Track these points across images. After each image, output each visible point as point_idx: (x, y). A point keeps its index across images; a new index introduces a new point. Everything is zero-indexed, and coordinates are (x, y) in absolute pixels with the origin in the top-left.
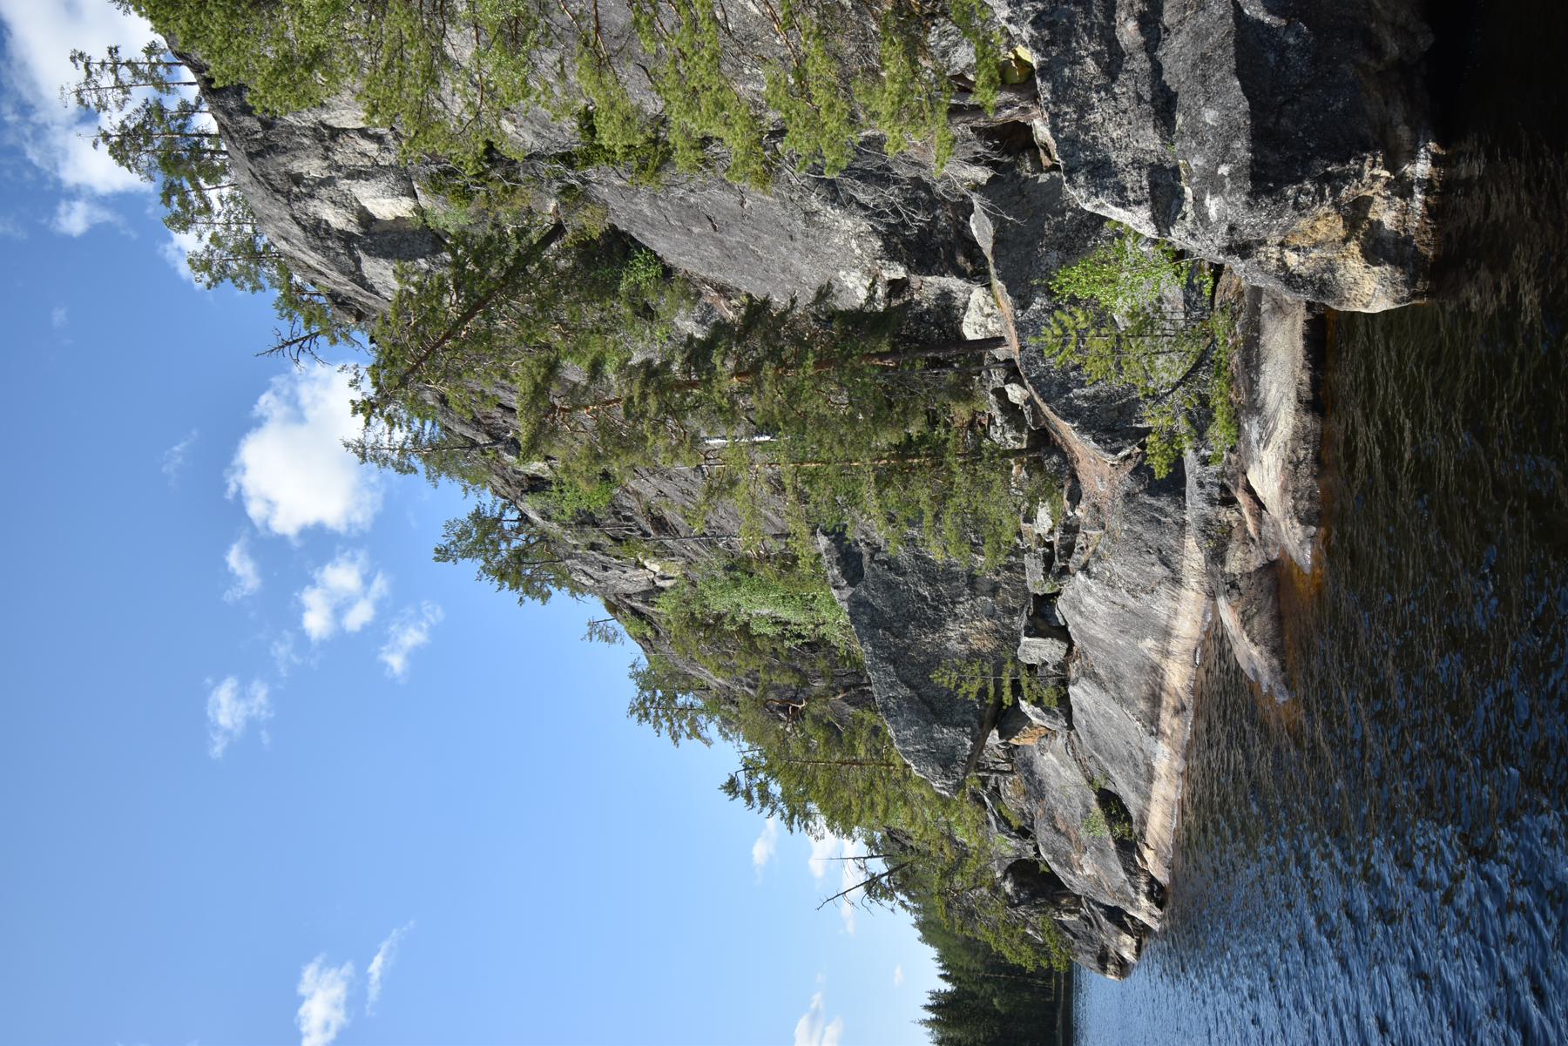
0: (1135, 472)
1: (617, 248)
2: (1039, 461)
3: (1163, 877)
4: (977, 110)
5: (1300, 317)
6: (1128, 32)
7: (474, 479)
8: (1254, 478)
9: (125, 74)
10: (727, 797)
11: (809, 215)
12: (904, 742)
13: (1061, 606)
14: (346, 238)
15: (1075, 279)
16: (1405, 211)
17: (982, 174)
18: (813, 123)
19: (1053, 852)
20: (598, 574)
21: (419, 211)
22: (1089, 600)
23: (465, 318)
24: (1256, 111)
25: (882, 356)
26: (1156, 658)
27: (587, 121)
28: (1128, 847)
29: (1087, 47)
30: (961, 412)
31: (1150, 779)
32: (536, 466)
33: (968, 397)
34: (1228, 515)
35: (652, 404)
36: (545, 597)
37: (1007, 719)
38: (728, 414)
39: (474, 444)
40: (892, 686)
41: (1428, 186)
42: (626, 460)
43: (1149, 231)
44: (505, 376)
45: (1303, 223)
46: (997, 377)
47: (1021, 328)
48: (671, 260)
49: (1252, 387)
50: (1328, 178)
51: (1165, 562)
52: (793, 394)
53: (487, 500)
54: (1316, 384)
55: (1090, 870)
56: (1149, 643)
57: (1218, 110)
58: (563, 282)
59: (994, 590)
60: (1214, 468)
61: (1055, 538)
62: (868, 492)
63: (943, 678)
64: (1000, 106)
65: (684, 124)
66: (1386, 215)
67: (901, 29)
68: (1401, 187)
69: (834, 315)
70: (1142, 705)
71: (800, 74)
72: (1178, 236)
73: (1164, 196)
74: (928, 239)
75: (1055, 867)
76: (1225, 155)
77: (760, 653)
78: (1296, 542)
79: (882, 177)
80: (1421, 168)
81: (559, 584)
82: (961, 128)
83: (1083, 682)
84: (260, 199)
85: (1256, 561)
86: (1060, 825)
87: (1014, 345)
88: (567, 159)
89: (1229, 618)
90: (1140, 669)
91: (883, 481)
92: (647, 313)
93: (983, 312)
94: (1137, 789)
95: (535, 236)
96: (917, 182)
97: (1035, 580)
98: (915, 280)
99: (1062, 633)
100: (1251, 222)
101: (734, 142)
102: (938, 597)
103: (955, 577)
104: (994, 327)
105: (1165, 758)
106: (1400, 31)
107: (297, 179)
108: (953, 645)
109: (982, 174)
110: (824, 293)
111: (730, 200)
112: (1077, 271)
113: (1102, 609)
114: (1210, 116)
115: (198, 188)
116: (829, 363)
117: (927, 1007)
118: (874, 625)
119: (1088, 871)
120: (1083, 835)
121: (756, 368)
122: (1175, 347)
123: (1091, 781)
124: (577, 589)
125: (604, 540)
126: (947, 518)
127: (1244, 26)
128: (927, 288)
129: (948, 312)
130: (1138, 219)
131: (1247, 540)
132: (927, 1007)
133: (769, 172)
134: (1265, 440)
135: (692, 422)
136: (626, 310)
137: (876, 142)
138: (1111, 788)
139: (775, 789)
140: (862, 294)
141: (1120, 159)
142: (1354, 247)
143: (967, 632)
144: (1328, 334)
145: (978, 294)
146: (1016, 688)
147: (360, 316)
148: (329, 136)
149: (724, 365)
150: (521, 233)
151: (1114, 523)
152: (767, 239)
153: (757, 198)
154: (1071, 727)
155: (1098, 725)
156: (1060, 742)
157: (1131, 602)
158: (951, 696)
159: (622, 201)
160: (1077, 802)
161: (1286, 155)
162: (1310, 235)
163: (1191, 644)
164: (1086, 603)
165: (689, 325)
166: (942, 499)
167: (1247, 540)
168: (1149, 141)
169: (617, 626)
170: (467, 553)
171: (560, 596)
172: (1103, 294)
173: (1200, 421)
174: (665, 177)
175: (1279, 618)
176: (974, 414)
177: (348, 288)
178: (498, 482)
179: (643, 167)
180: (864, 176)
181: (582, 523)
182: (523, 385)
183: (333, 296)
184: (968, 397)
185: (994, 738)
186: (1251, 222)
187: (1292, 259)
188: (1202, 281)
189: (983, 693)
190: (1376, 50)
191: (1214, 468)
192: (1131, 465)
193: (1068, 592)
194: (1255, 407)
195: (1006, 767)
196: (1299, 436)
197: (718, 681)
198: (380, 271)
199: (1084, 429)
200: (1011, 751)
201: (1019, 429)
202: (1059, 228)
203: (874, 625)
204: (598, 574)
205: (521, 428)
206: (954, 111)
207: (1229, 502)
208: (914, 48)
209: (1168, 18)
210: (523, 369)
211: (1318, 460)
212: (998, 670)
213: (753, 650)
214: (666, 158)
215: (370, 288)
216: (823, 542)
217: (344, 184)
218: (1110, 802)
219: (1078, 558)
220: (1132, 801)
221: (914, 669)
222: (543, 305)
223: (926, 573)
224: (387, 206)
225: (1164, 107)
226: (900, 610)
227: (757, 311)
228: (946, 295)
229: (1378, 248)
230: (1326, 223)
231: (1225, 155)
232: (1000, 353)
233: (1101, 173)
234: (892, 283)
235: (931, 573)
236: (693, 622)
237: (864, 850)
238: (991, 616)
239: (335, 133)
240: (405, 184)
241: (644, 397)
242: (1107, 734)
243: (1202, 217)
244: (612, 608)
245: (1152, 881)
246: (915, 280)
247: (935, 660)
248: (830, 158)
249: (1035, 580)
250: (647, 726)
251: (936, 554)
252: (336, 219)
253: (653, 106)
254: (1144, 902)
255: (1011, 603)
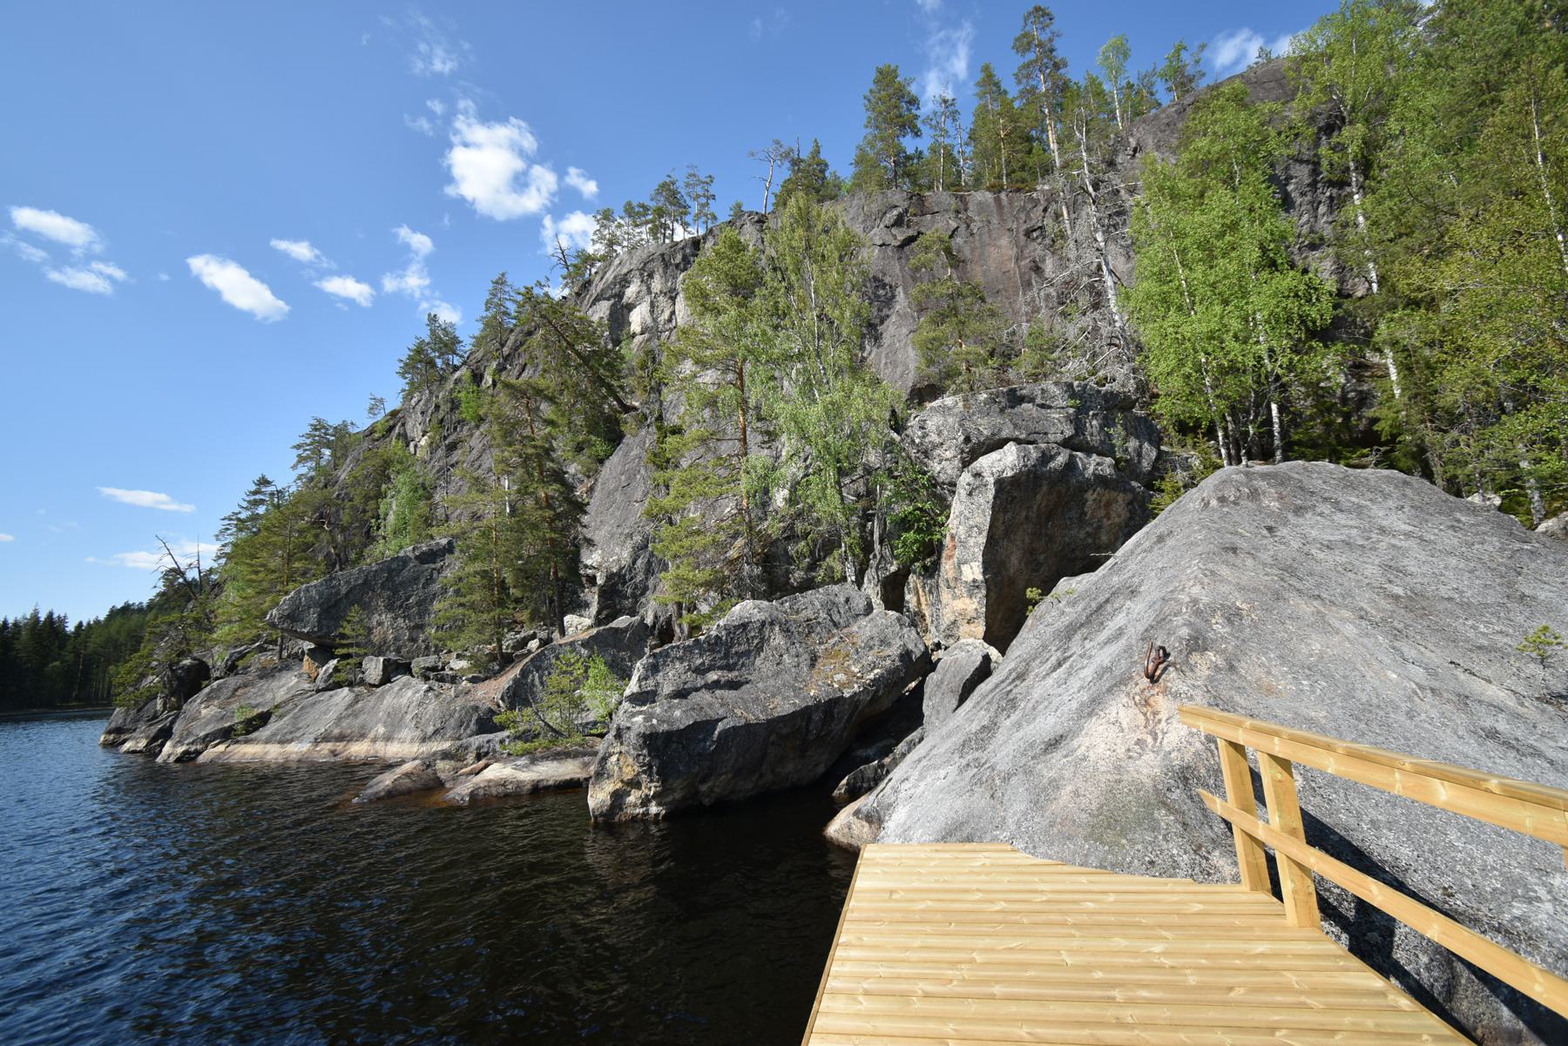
0: (490, 710)
1: (615, 438)
2: (495, 659)
3: (202, 759)
4: (680, 615)
5: (582, 775)
6: (713, 676)
7: (479, 342)
8: (495, 766)
9: (703, 200)
10: (256, 478)
11: (631, 536)
12: (307, 590)
13: (406, 678)
14: (620, 295)
15: (599, 667)
16: (635, 806)
17: (649, 620)
18: (675, 539)
19: (219, 688)
20: (419, 408)
21: (634, 335)
22: (410, 693)
23: (578, 354)
24: (680, 732)
25: (556, 573)
26: (371, 735)
27: (677, 431)
28: (226, 735)
29: (707, 659)
30: (524, 616)
31: (281, 742)
32: (488, 380)
33: (532, 619)
34: (471, 757)
35: (530, 451)
36: (403, 375)
37: (323, 652)
38: (523, 492)
39: (503, 346)
40: (347, 582)
41: (646, 814)
42: (498, 435)
43: (627, 692)
44: (545, 371)
45: (630, 760)
46: (543, 634)
47: (572, 644)
48: (607, 463)
49: (546, 758)
50: (651, 767)
51: (436, 732)
52: (535, 526)
53: (467, 345)
54: (547, 788)
55: (204, 712)
56: (381, 730)
57: (680, 716)
58: (596, 406)
59: (413, 640)
60: (498, 747)
61: (447, 671)
62: (478, 566)
63: (354, 613)
64: (681, 627)
65: (676, 476)
66: (634, 797)
67: (716, 579)
68: (645, 802)
69: (578, 548)
70: (336, 731)
71: (698, 533)
72: (626, 705)
73: (642, 698)
74: (617, 593)
75: (207, 690)
76: (661, 721)
77: (366, 503)
78: (461, 791)
79: (649, 571)
80: (654, 809)
81: (411, 383)
82: (672, 609)
83: (352, 695)
84: (640, 255)
85: (442, 776)
86: (240, 692)
87: (562, 641)
88: (660, 418)
89: (407, 767)
90: (362, 727)
91: (485, 574)
92: (579, 449)
93: (578, 625)
94: (274, 735)
95: (621, 394)
96: (646, 589)
97: (419, 663)
98: (595, 589)
99: (386, 679)
100: (631, 737)
101: (667, 502)
102: (408, 608)
103: (421, 615)
104: (570, 631)
105: (297, 749)
106: (711, 789)
107: (651, 276)
108: (376, 618)
109: (649, 620)
110: (590, 542)
111: (638, 495)
112: (602, 667)
113: (404, 701)
114: (678, 713)
115: (647, 222)
116: (553, 545)
117: (51, 614)
118: (390, 571)
119: (204, 712)
120: (235, 706)
121: (550, 506)
122: (564, 720)
123: (277, 707)
124: (408, 396)
125: (441, 414)
126: (461, 610)
127: (713, 723)
128: (592, 597)
129: (578, 606)
130: (633, 687)
131: (456, 770)
132: (51, 614)
133: (652, 517)
134: (517, 768)
135: (520, 472)
136: (581, 438)
137: (665, 568)
138: (273, 718)
139: (261, 510)
140: (589, 562)
141: (659, 677)
142: (619, 785)
143: (384, 624)
144: (575, 788)
145: (588, 622)
146: (348, 656)
147: (578, 294)
148: (672, 296)
149: (553, 489)
150: (622, 387)
151: (460, 702)
152: (618, 514)
153: (639, 510)
154: (318, 691)
155: (322, 707)
156: (306, 686)
157: (409, 717)
158: (343, 618)
159: (638, 442)
160: (260, 700)
161: (662, 749)
162: (625, 763)
163: (381, 754)
164: (408, 692)
165: (572, 469)
166: (473, 606)
167: (456, 770)
168: (667, 689)
169: (380, 417)
170: (433, 332)
171: (402, 384)
172: (591, 681)
173: (526, 736)
174: (651, 465)
175: (409, 792)
176: (522, 623)
177: (594, 290)
178: (479, 355)
179: (655, 455)
180: (649, 563)
181: (452, 401)
182: (542, 383)
183: (589, 282)
184: (532, 619)
185: (308, 646)
186: (631, 737)
187: (614, 759)
188: (596, 730)
189: (343, 636)
190: (703, 781)
191: (498, 747)
192: (494, 708)
193: (414, 681)
194: (534, 761)
195: (285, 654)
196: (519, 784)
197: (343, 475)
198: (601, 312)
199: (516, 681)
200: (298, 657)
201: (514, 648)
202: (623, 659)
203: (390, 571)
204: (419, 408)
205: (510, 377)
206: (679, 605)
207: (479, 757)
208: (708, 585)
209: (718, 692)
210: (549, 382)
211: (507, 795)
212: (358, 645)
213: (367, 498)
214: (660, 467)
215: (594, 303)
216: (444, 541)
217: (648, 299)
218: (264, 719)
219: (436, 685)
220: (265, 732)
221: (360, 595)
222: (583, 395)
223: (425, 600)
224: (637, 318)
225: (681, 694)
226: (401, 585)
227: (581, 508)
228: (587, 605)
229: (618, 797)
230: (628, 773)
231: (661, 721)
232: (556, 635)
233: (654, 669)
234: (594, 577)
235: (424, 605)
236: (387, 464)
237: (205, 566)
238: (395, 639)
239: (673, 299)
240: (651, 330)
241: (535, 447)
242: (314, 713)
243: (634, 715)
244: (394, 414)
245: (198, 753)
246: (595, 589)
247: (367, 608)
248: (659, 546)
249: (419, 663)
250: (308, 430)
251: (436, 605)
252: (631, 292)
253: (685, 464)
254: (180, 750)
255: (404, 650)
